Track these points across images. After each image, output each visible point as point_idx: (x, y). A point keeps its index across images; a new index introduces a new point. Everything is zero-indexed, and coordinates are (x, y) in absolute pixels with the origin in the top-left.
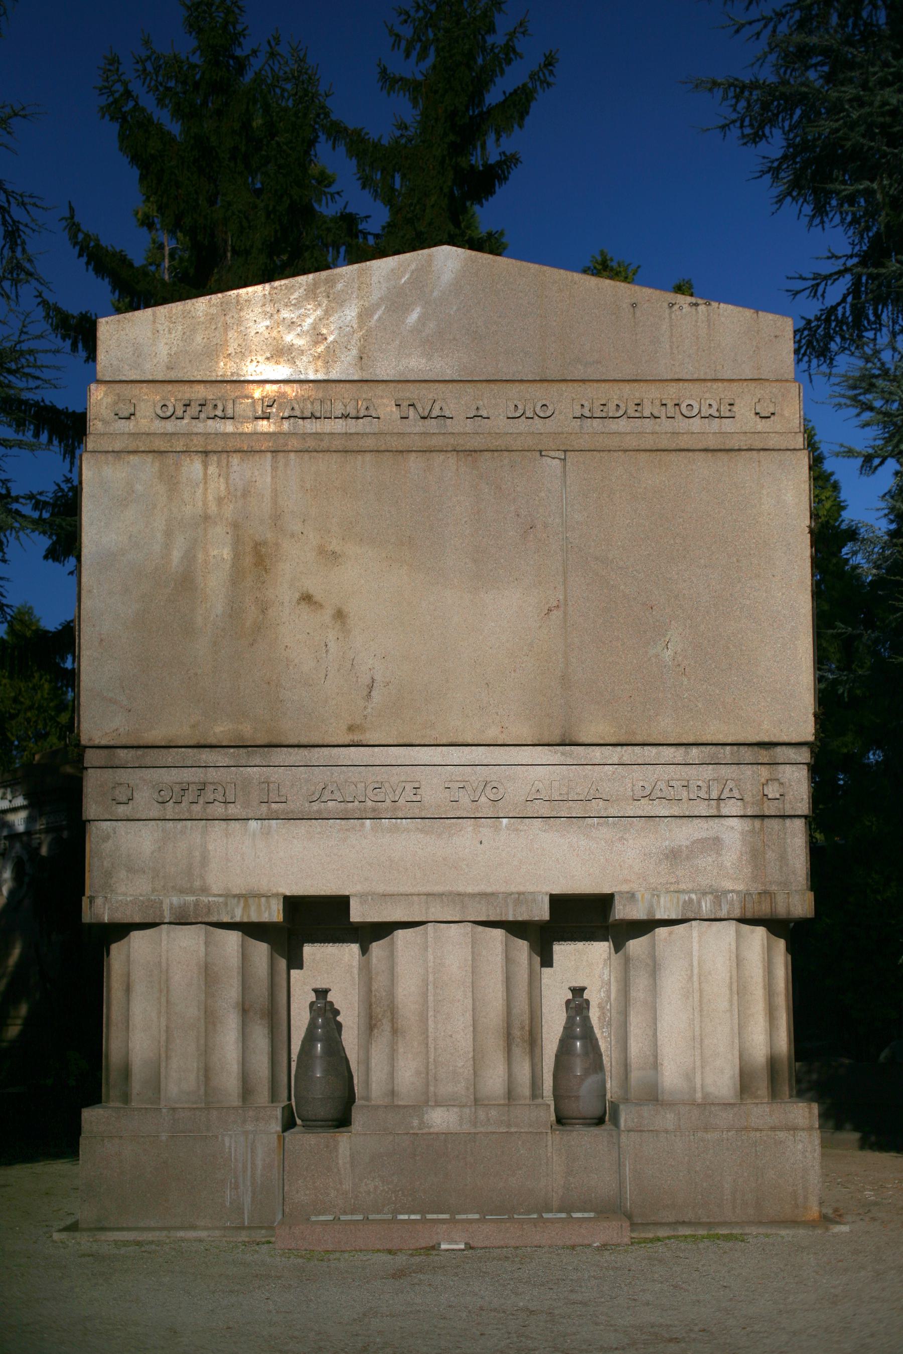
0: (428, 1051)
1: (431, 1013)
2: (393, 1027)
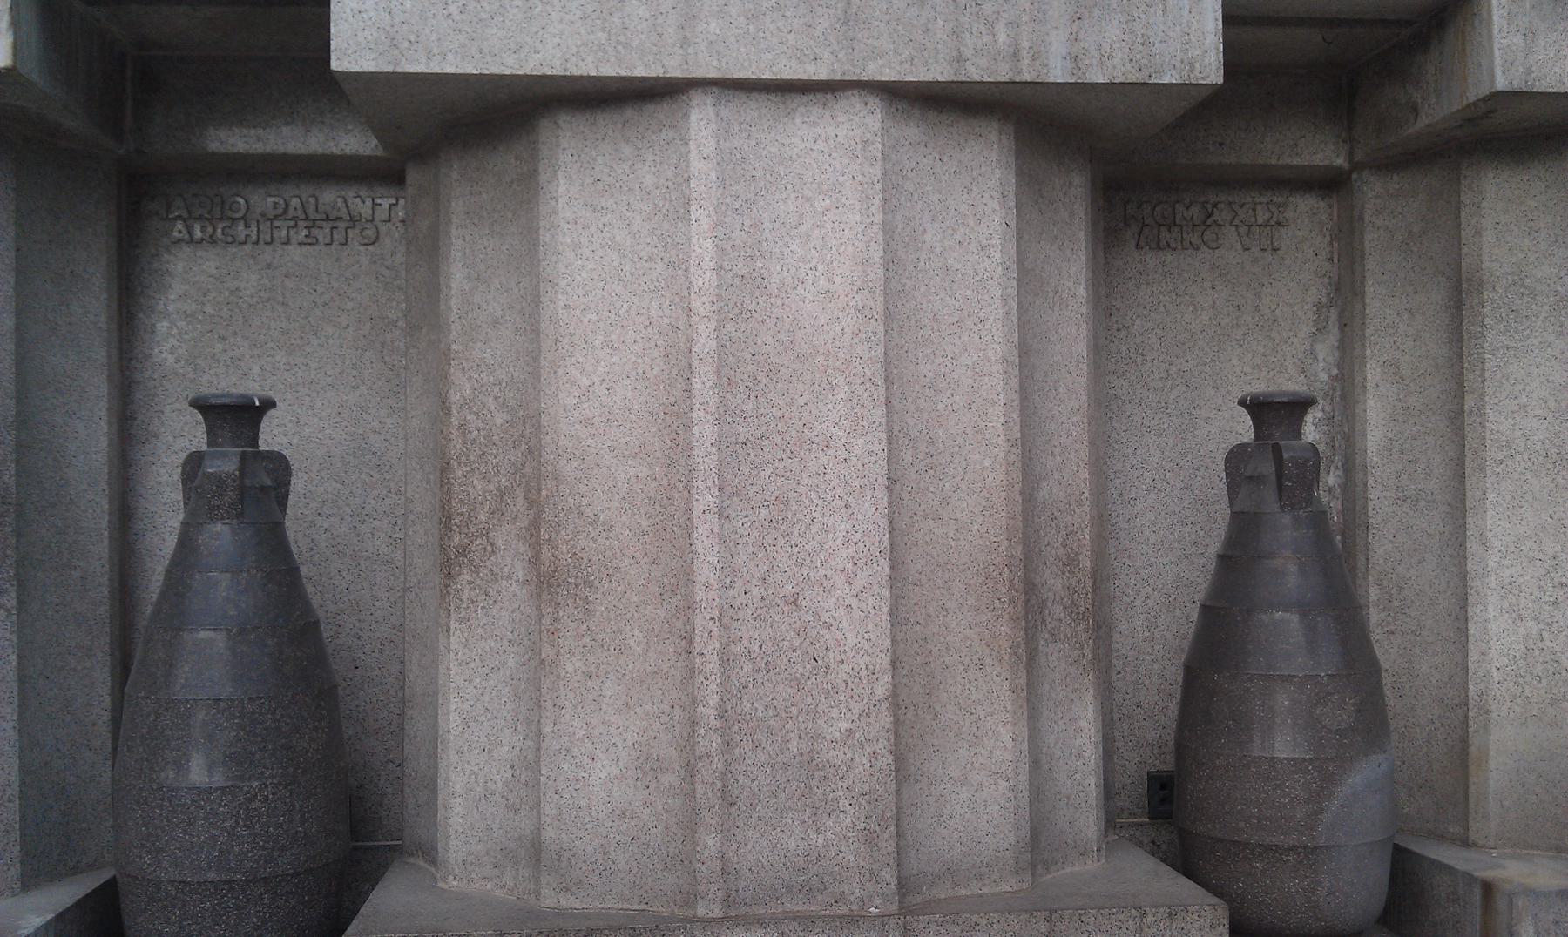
0: (691, 673)
1: (705, 501)
2: (535, 561)
